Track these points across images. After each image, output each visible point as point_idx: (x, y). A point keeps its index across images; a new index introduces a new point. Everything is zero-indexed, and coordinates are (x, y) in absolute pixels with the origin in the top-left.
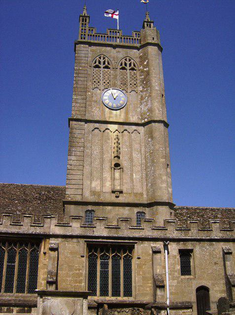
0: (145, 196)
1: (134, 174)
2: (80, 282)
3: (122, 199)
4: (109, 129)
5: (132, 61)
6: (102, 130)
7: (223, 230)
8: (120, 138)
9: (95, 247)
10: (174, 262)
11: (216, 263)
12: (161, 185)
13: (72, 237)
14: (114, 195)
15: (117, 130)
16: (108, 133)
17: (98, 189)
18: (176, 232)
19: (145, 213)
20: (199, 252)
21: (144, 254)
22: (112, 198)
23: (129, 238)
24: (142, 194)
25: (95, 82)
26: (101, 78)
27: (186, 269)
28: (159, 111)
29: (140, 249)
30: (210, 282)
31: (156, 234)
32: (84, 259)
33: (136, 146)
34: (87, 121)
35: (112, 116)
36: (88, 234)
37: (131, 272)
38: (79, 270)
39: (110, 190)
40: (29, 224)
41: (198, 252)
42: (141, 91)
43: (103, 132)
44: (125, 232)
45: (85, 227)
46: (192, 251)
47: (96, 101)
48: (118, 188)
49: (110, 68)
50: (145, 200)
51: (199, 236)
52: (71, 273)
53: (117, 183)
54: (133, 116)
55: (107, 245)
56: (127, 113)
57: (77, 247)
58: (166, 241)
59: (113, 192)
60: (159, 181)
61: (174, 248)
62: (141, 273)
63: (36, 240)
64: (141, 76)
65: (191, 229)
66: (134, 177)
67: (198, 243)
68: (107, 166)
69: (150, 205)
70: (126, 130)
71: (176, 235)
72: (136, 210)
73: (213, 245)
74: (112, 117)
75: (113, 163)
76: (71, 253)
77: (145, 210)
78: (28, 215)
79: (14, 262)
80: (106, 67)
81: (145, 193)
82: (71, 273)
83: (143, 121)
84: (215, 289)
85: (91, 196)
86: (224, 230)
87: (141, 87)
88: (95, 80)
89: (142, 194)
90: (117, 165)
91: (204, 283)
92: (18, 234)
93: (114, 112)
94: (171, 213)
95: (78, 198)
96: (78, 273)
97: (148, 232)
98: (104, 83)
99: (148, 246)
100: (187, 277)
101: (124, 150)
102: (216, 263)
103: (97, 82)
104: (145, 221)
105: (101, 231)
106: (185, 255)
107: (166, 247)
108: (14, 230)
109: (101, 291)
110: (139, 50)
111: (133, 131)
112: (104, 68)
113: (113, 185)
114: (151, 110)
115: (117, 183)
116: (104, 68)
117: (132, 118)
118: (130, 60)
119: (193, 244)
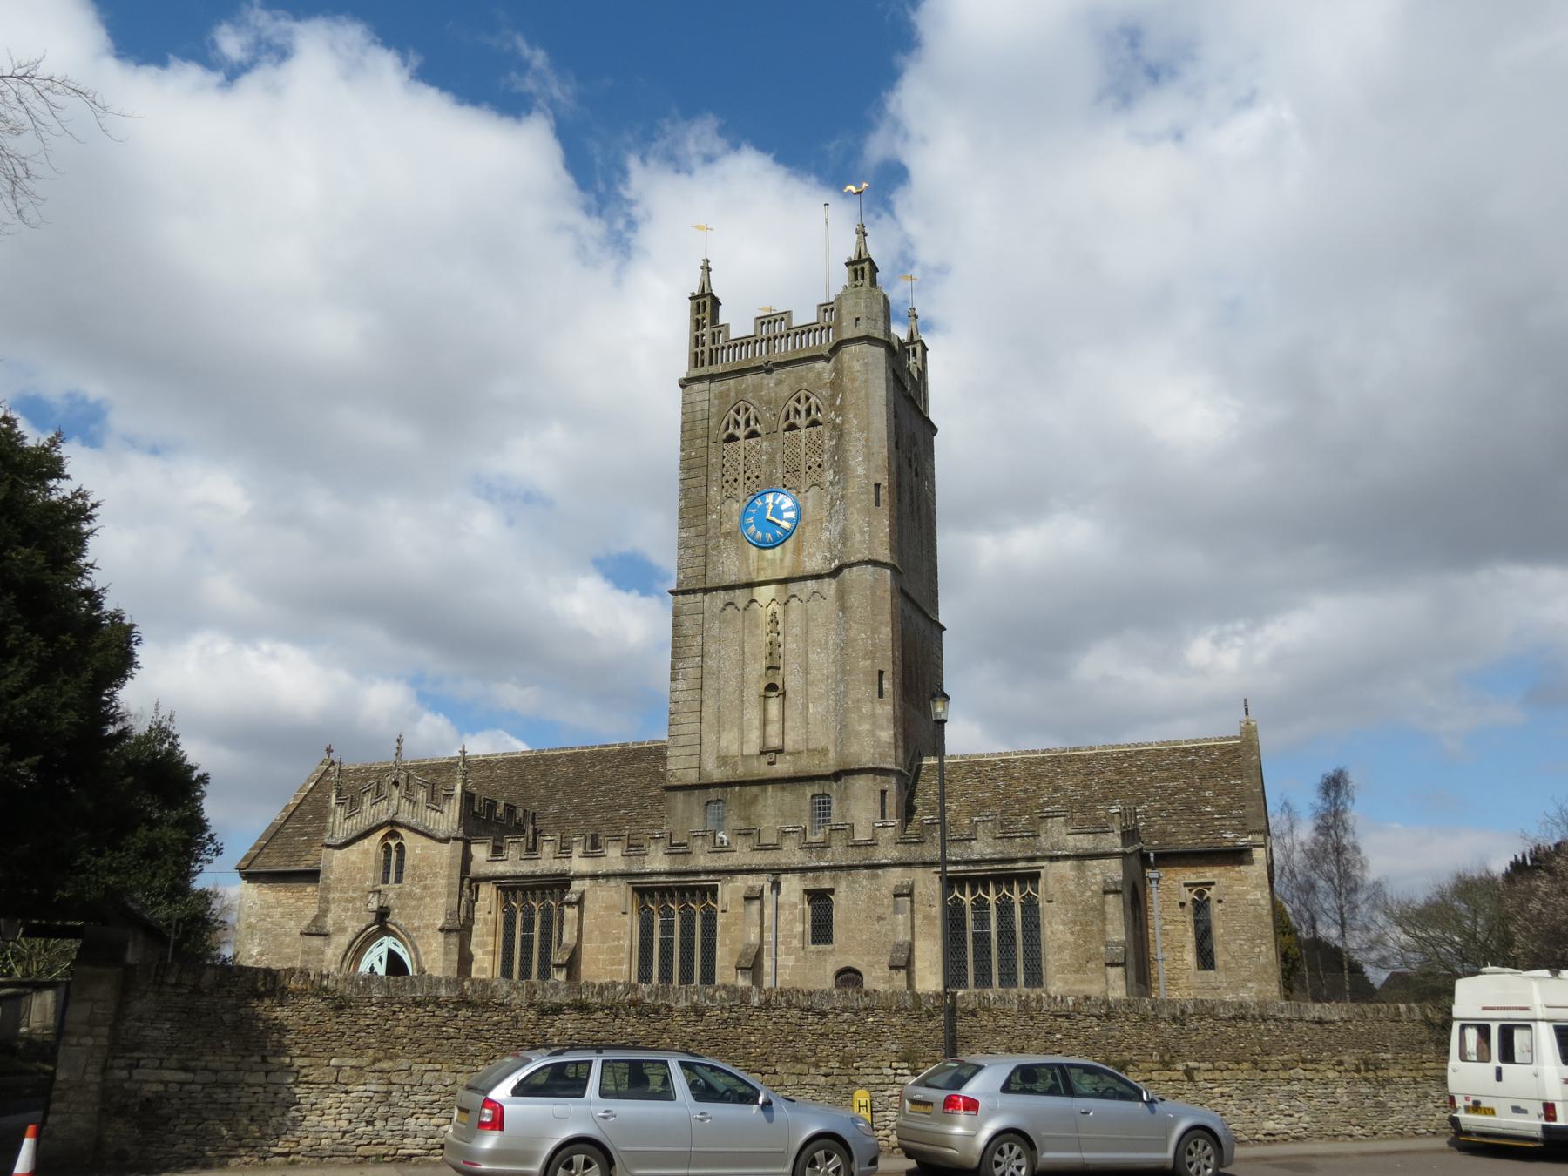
0: (832, 755)
1: (811, 705)
2: (620, 963)
3: (783, 767)
4: (756, 601)
5: (813, 400)
6: (741, 606)
7: (903, 841)
8: (780, 618)
9: (646, 891)
10: (791, 917)
11: (880, 918)
12: (858, 728)
13: (606, 876)
14: (765, 759)
15: (774, 600)
16: (755, 611)
17: (734, 749)
18: (799, 853)
19: (828, 795)
20: (848, 897)
21: (734, 904)
22: (762, 769)
23: (708, 872)
24: (825, 751)
25: (727, 482)
26: (741, 471)
27: (822, 930)
28: (862, 533)
29: (729, 892)
30: (866, 959)
31: (760, 859)
32: (627, 918)
33: (817, 633)
34: (706, 591)
35: (765, 564)
36: (635, 869)
37: (714, 935)
38: (619, 939)
39: (756, 751)
40: (552, 855)
41: (843, 894)
42: (832, 484)
43: (745, 609)
44: (702, 860)
45: (630, 856)
46: (831, 891)
47: (727, 535)
48: (774, 742)
49: (760, 435)
50: (831, 766)
51: (847, 859)
52: (605, 946)
53: (774, 729)
54: (811, 555)
55: (670, 887)
56: (798, 550)
57: (616, 896)
58: (776, 872)
59: (763, 753)
60: (854, 717)
61: (793, 887)
62: (728, 942)
63: (560, 883)
64: (831, 440)
65: (833, 843)
66: (811, 710)
67: (844, 874)
68: (754, 690)
69: (837, 776)
70: (795, 596)
71: (798, 858)
72: (809, 790)
73: (877, 876)
74: (763, 569)
75: (763, 684)
76: (607, 908)
77: (831, 787)
78: (549, 838)
79: (532, 930)
80: (753, 434)
81: (831, 748)
82: (605, 946)
83: (833, 566)
84: (874, 974)
85: (718, 767)
86: (906, 843)
87: (831, 472)
88: (726, 477)
89: (825, 751)
90: (772, 687)
91: (852, 961)
92: (533, 876)
93: (769, 553)
94: (883, 793)
95: (692, 777)
96: (617, 946)
97: (742, 855)
98: (749, 479)
99: (742, 883)
100: (821, 947)
101: (791, 645)
102: (880, 918)
103: (731, 479)
104: (740, 834)
105: (657, 861)
106: (820, 900)
107: (776, 886)
108: (526, 868)
109: (989, 939)
110: (828, 360)
111: (809, 594)
112: (747, 437)
113: (764, 737)
114: (844, 536)
115: (774, 729)
116: (747, 437)
117: (810, 560)
118: (807, 399)
119: (833, 879)
